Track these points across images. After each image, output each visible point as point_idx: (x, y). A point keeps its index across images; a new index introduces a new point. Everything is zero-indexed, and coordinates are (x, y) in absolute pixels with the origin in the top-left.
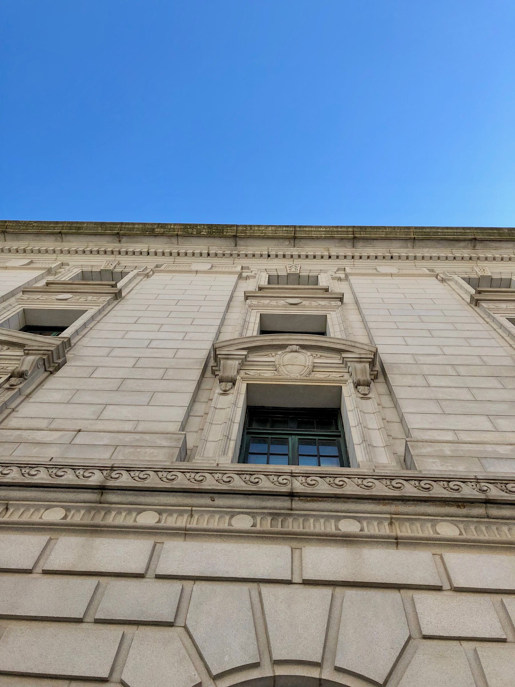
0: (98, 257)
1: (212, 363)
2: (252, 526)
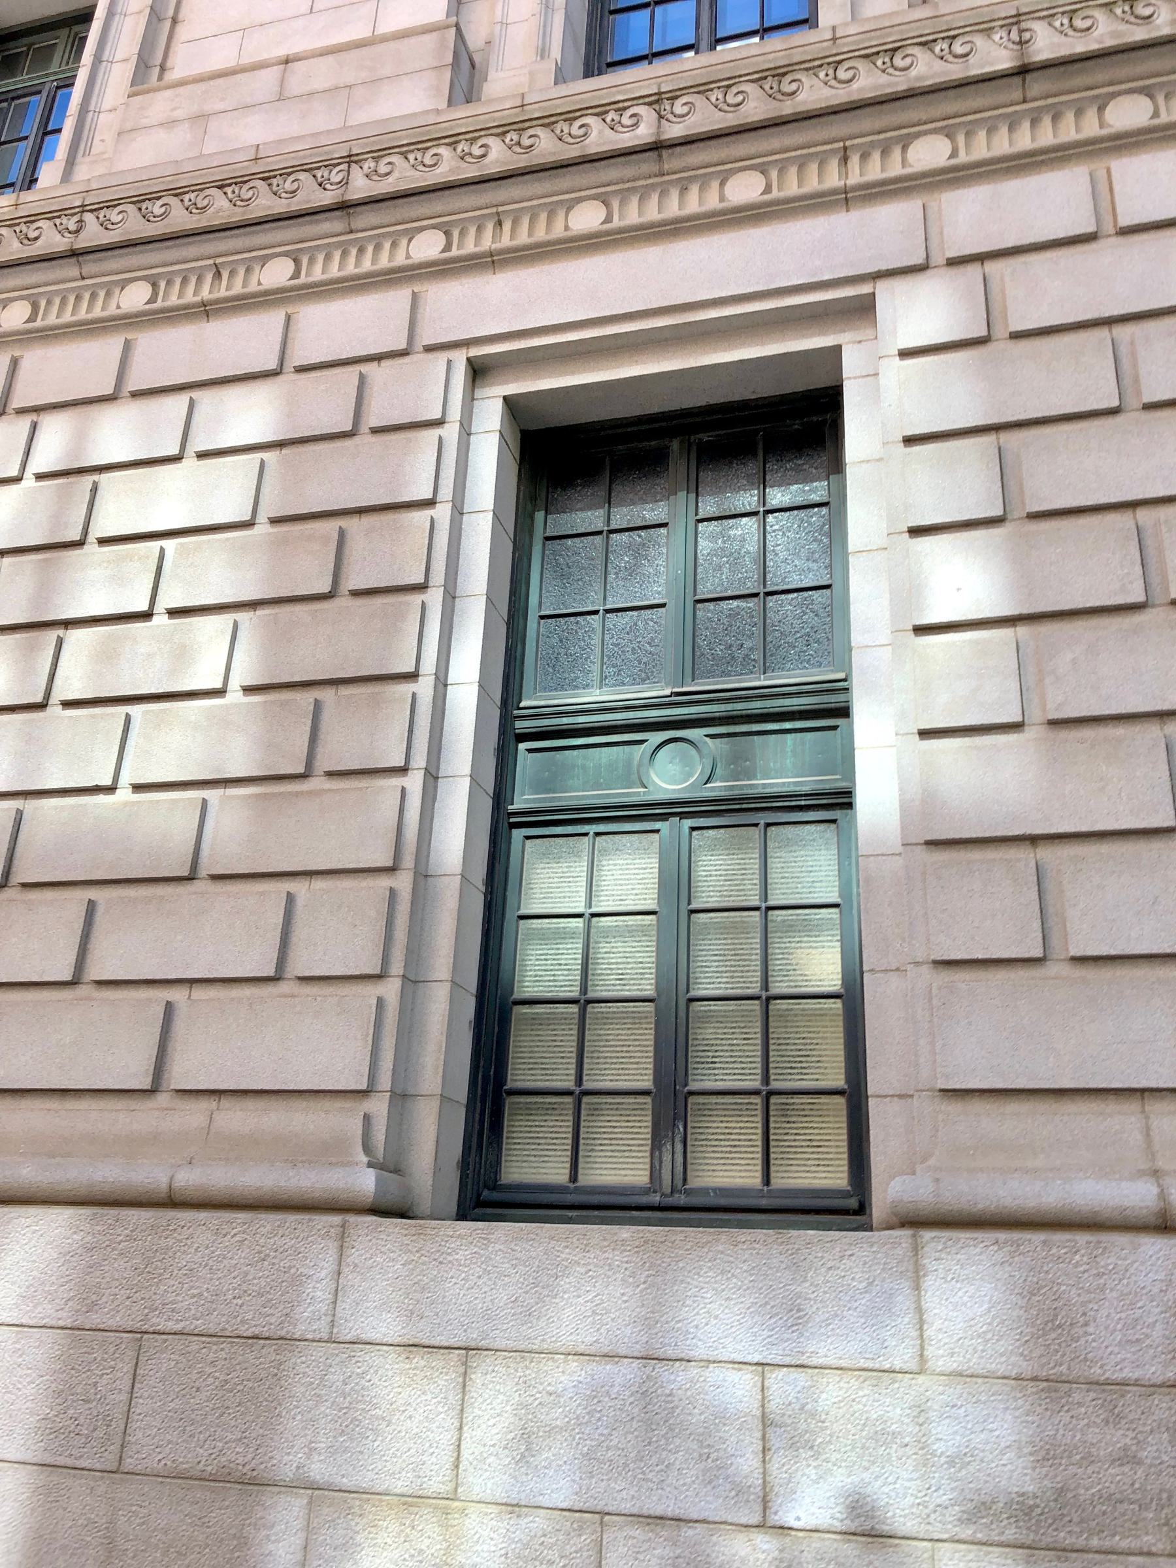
2: (1152, 118)
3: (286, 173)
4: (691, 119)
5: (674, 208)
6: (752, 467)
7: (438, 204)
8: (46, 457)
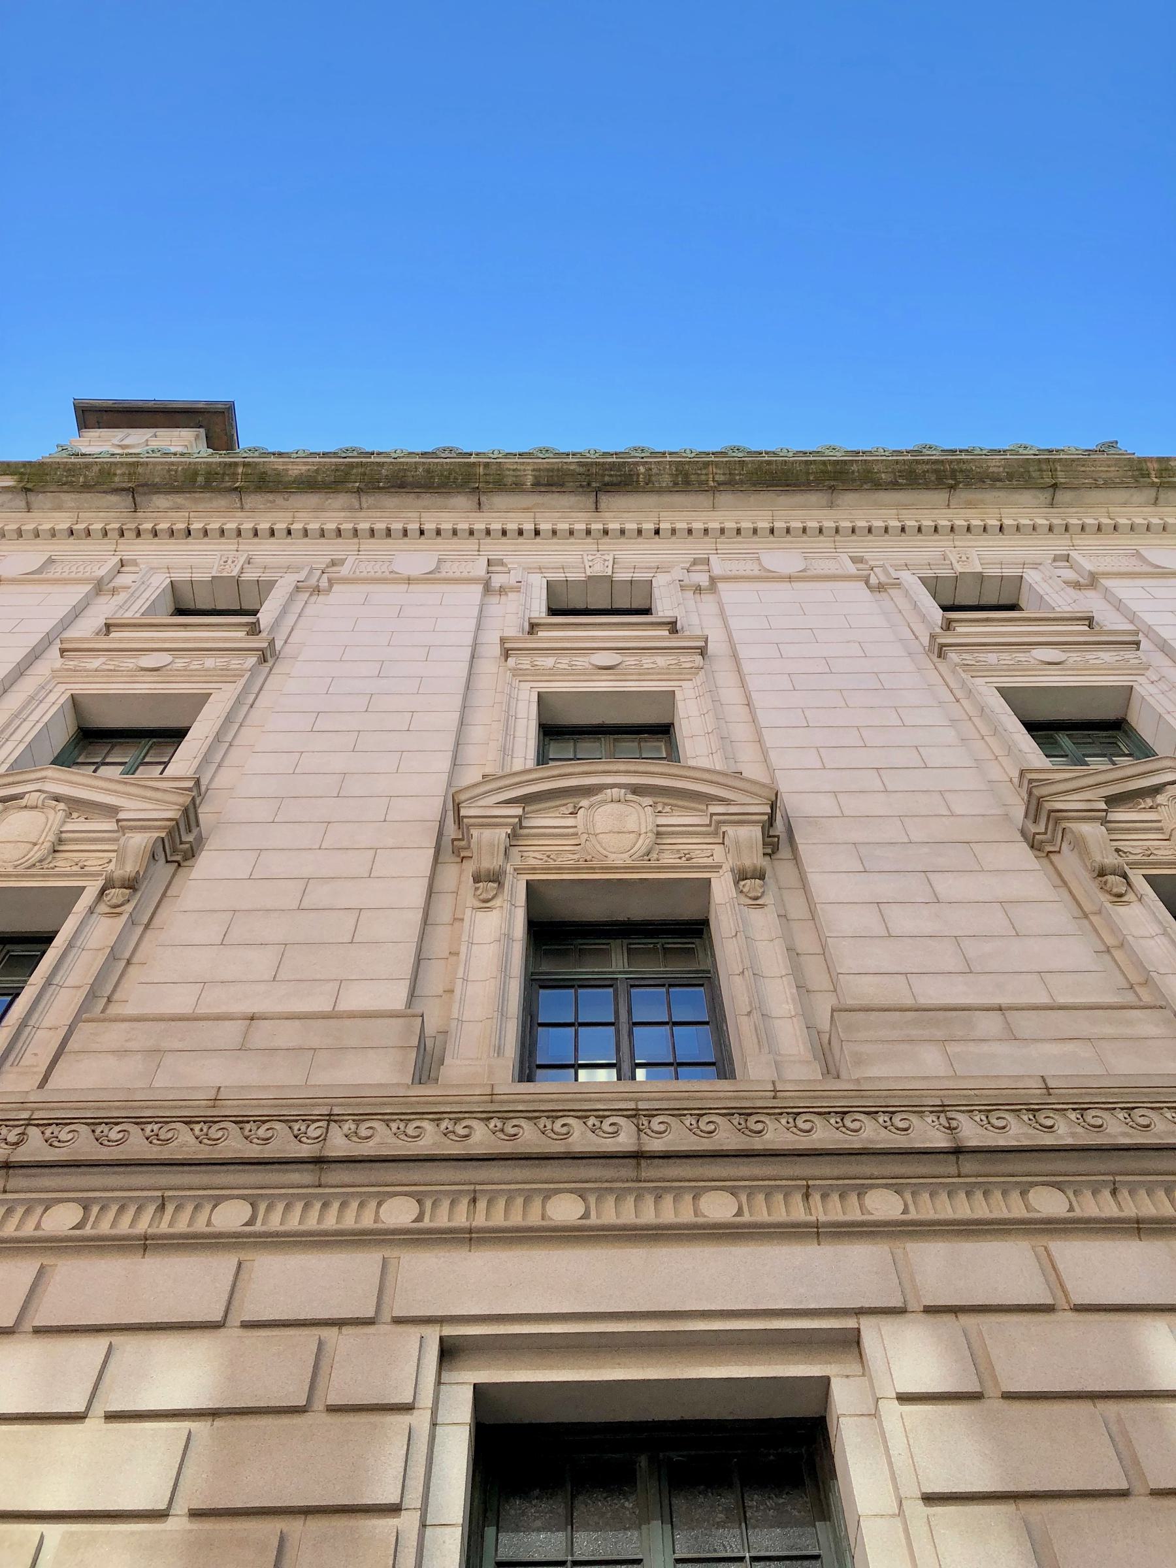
0: (322, 544)
1: (451, 830)
3: (262, 1121)
4: (668, 1137)
5: (648, 1215)
6: (728, 1500)
7: (416, 1174)
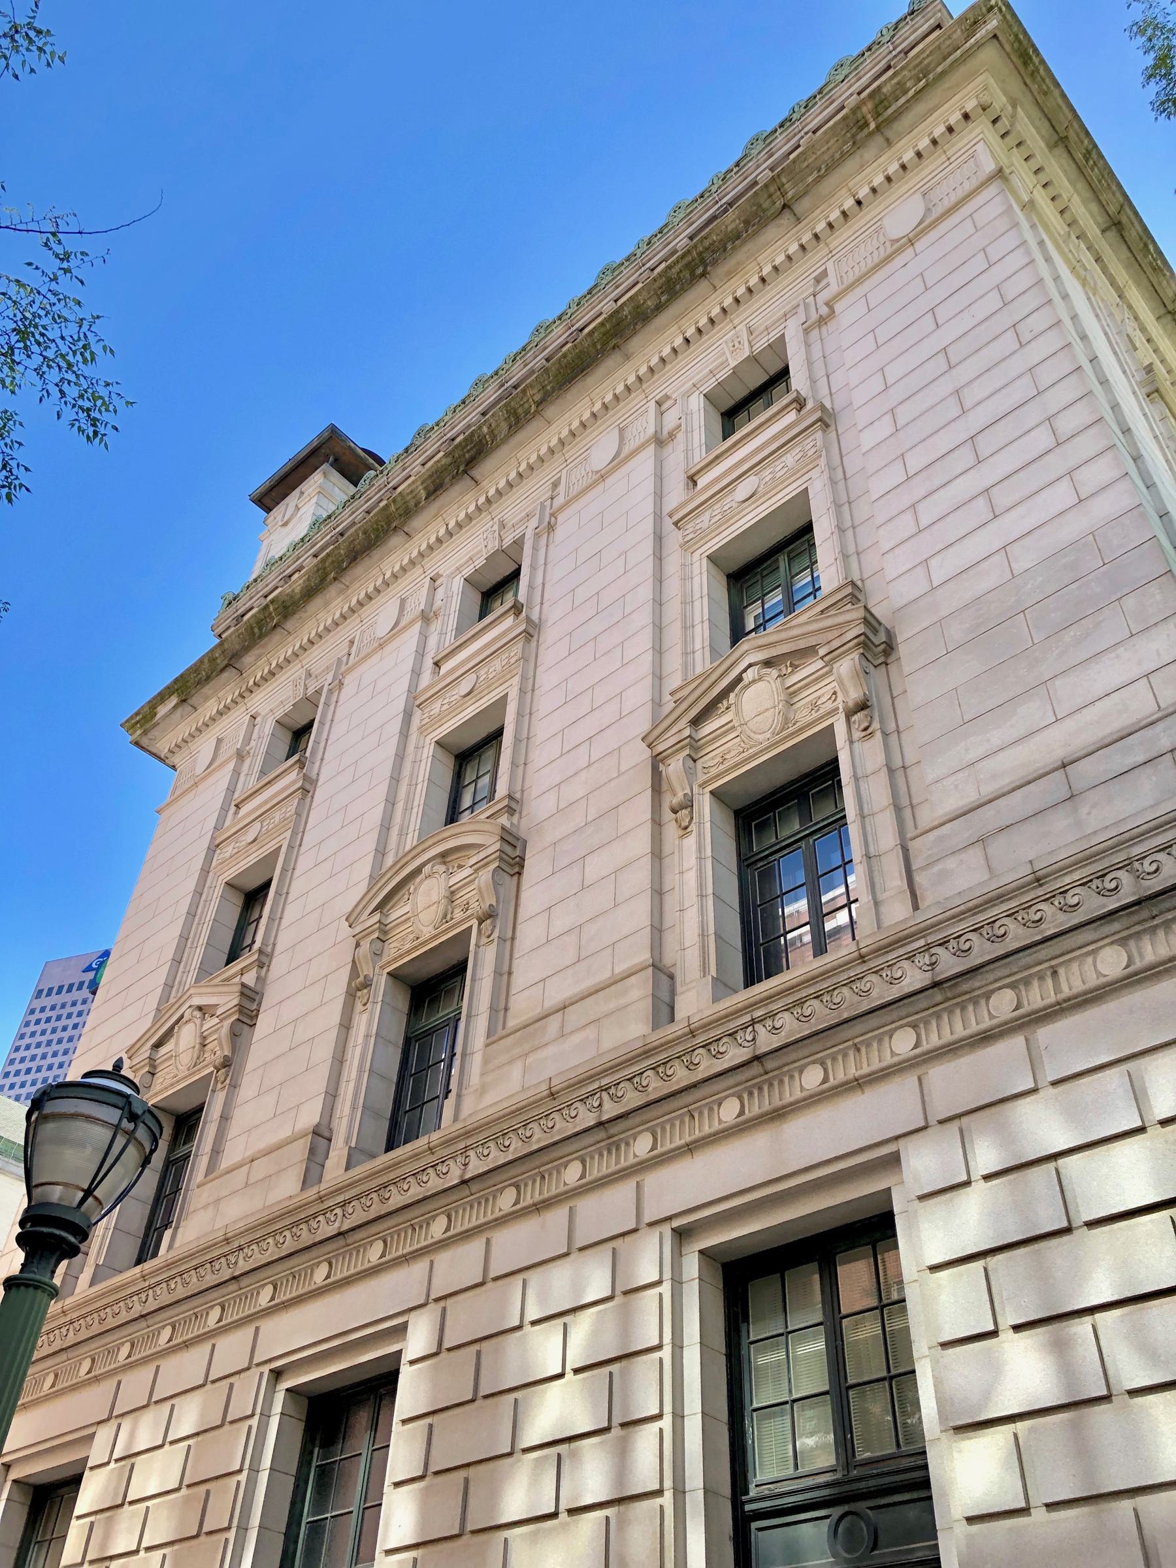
8: (987, 1157)
